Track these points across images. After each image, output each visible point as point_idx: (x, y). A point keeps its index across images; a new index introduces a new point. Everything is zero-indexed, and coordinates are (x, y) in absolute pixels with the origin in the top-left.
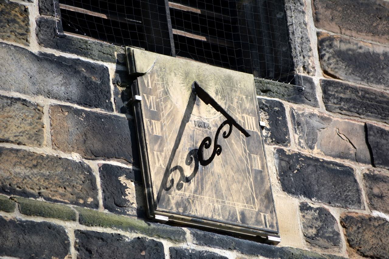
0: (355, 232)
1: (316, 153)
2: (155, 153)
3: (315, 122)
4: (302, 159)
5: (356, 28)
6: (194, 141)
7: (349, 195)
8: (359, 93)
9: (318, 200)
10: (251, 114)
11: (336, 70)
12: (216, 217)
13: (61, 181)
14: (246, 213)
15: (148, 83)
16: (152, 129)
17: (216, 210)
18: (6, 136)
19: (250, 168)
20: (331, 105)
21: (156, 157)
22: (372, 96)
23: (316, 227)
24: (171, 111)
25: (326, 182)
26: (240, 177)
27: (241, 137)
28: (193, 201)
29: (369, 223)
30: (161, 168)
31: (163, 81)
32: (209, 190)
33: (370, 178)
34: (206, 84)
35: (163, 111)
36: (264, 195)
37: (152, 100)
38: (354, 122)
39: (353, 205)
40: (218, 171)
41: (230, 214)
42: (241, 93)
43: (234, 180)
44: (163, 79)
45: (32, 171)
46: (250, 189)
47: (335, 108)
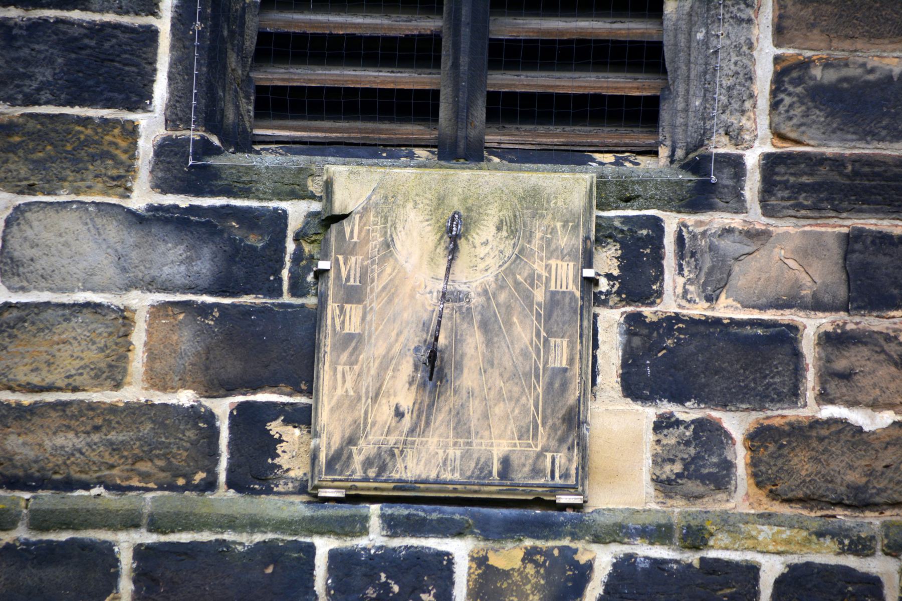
0: (771, 456)
1: (726, 309)
2: (340, 368)
3: (727, 245)
4: (681, 325)
5: (867, 31)
6: (428, 333)
7: (775, 383)
8: (845, 167)
9: (699, 405)
10: (567, 258)
11: (803, 128)
12: (447, 476)
13: (146, 449)
14: (515, 461)
15: (352, 232)
16: (343, 322)
17: (449, 462)
18: (49, 379)
19: (541, 367)
20: (775, 203)
21: (339, 376)
22: (877, 169)
23: (683, 459)
24: (390, 280)
25: (727, 364)
26: (516, 390)
27: (535, 306)
28: (402, 452)
29: (809, 434)
30: (347, 395)
31: (386, 223)
32: (441, 425)
33: (832, 341)
34: (480, 213)
35: (373, 281)
36: (560, 416)
37: (353, 265)
38: (823, 229)
39: (779, 401)
40: (470, 383)
41: (477, 464)
42: (554, 218)
43: (500, 397)
44: (386, 218)
45: (89, 440)
46: (533, 408)
47: (784, 207)
